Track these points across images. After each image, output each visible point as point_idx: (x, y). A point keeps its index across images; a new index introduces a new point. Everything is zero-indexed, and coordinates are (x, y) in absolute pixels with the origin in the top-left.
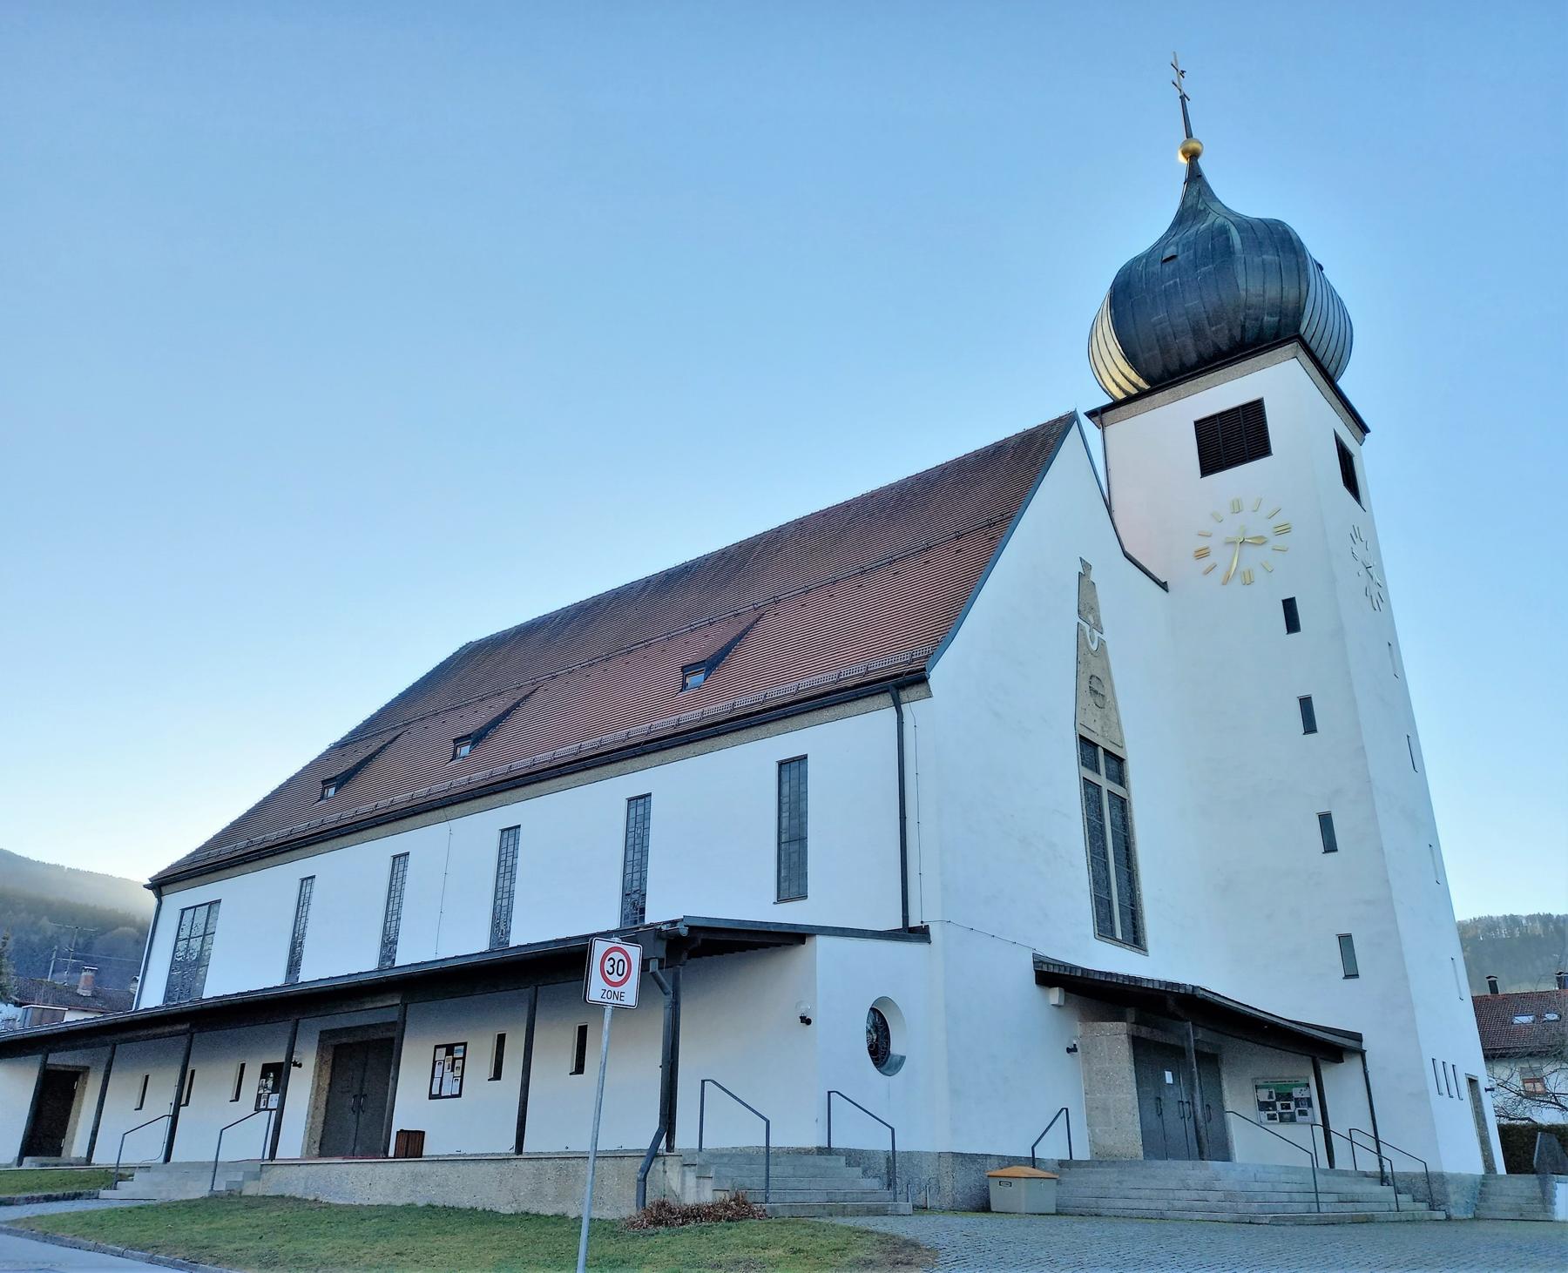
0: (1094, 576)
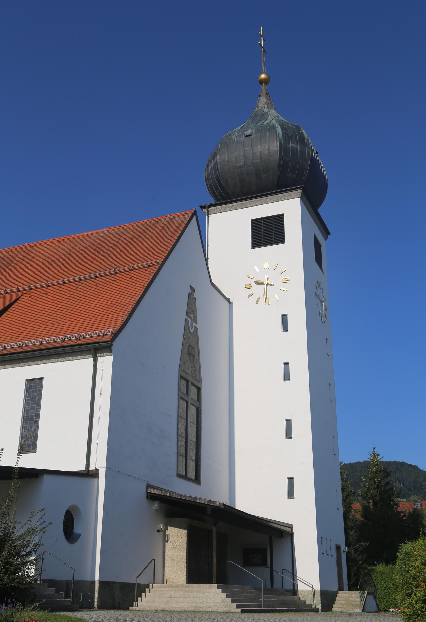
0: (196, 295)
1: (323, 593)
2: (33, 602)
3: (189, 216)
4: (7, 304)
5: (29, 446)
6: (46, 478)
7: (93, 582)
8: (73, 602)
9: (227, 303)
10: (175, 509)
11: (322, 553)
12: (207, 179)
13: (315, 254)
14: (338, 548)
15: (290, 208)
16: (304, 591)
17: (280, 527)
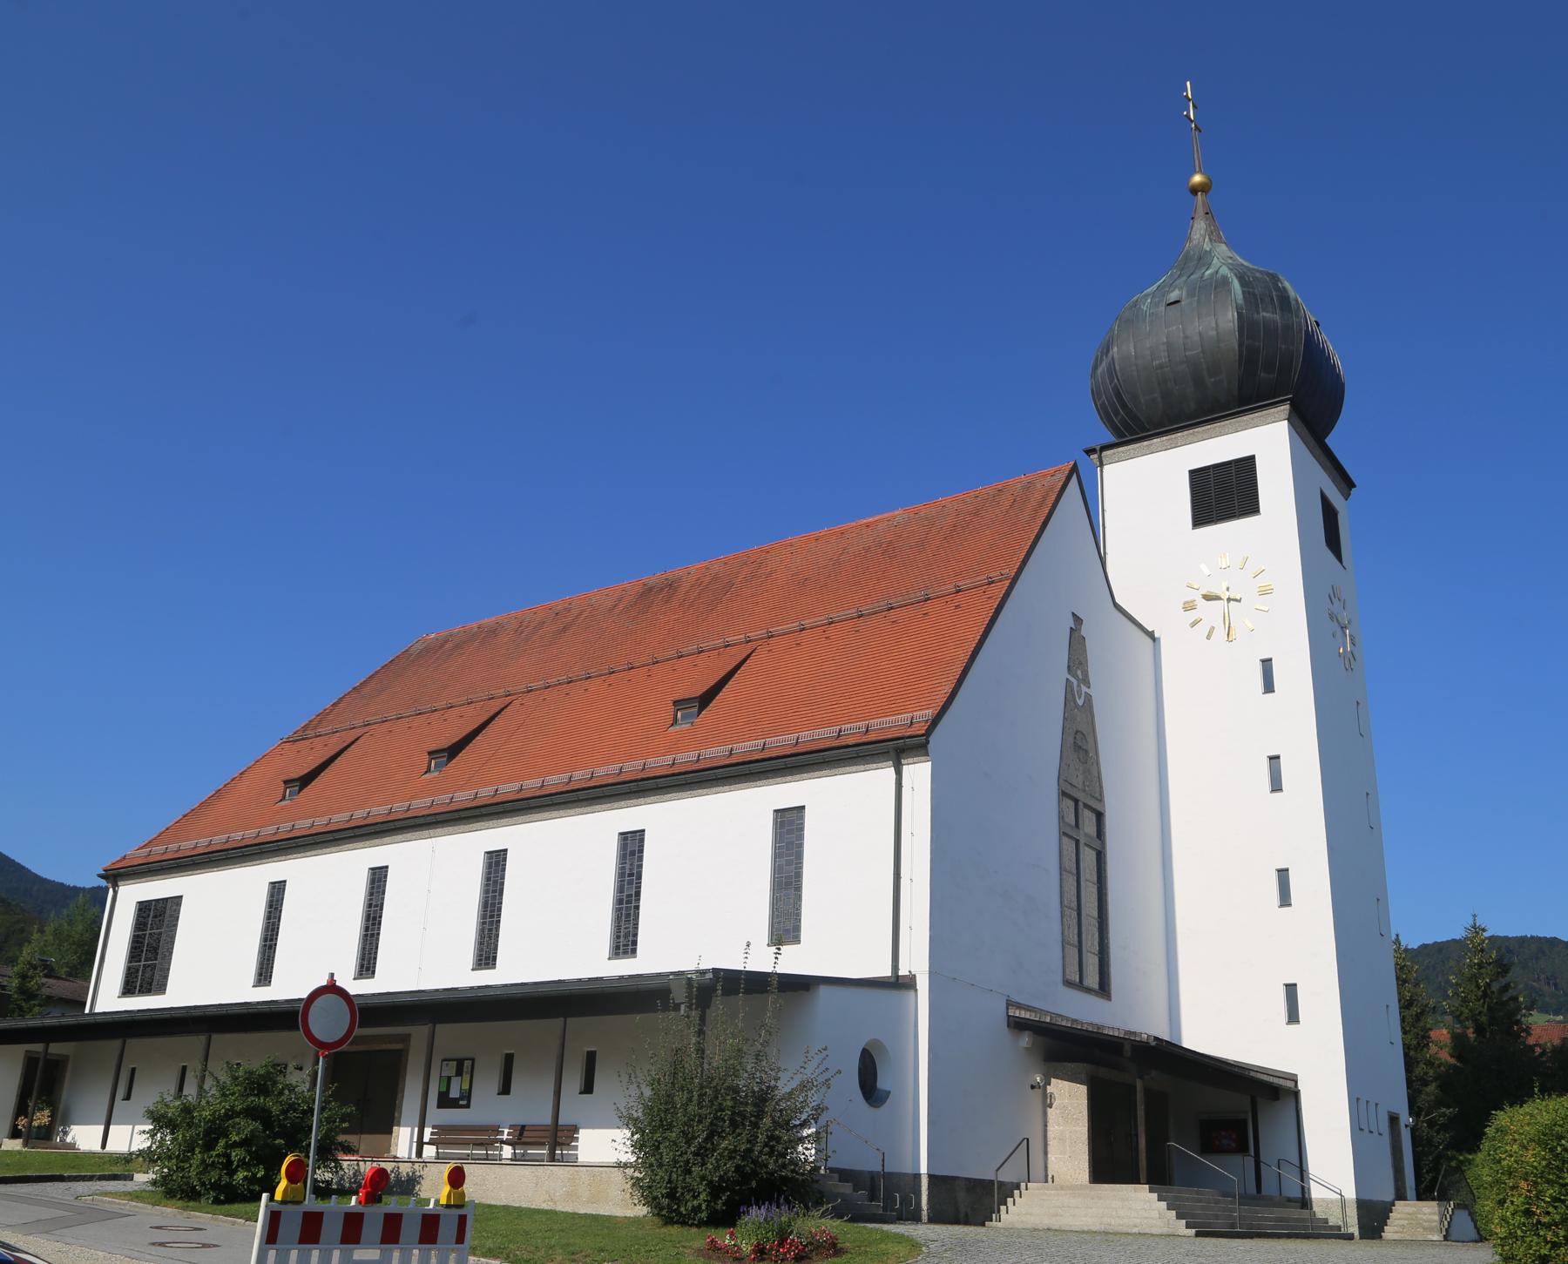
1: (1362, 1205)
2: (818, 1203)
3: (1062, 477)
4: (729, 668)
5: (787, 931)
6: (823, 990)
7: (918, 1176)
8: (885, 1209)
9: (1149, 641)
10: (1064, 1048)
11: (1359, 1129)
12: (1095, 394)
13: (1327, 530)
14: (1394, 1119)
15: (1267, 442)
16: (1323, 1200)
17: (1271, 1079)
